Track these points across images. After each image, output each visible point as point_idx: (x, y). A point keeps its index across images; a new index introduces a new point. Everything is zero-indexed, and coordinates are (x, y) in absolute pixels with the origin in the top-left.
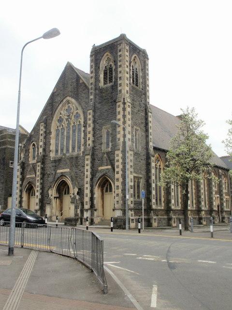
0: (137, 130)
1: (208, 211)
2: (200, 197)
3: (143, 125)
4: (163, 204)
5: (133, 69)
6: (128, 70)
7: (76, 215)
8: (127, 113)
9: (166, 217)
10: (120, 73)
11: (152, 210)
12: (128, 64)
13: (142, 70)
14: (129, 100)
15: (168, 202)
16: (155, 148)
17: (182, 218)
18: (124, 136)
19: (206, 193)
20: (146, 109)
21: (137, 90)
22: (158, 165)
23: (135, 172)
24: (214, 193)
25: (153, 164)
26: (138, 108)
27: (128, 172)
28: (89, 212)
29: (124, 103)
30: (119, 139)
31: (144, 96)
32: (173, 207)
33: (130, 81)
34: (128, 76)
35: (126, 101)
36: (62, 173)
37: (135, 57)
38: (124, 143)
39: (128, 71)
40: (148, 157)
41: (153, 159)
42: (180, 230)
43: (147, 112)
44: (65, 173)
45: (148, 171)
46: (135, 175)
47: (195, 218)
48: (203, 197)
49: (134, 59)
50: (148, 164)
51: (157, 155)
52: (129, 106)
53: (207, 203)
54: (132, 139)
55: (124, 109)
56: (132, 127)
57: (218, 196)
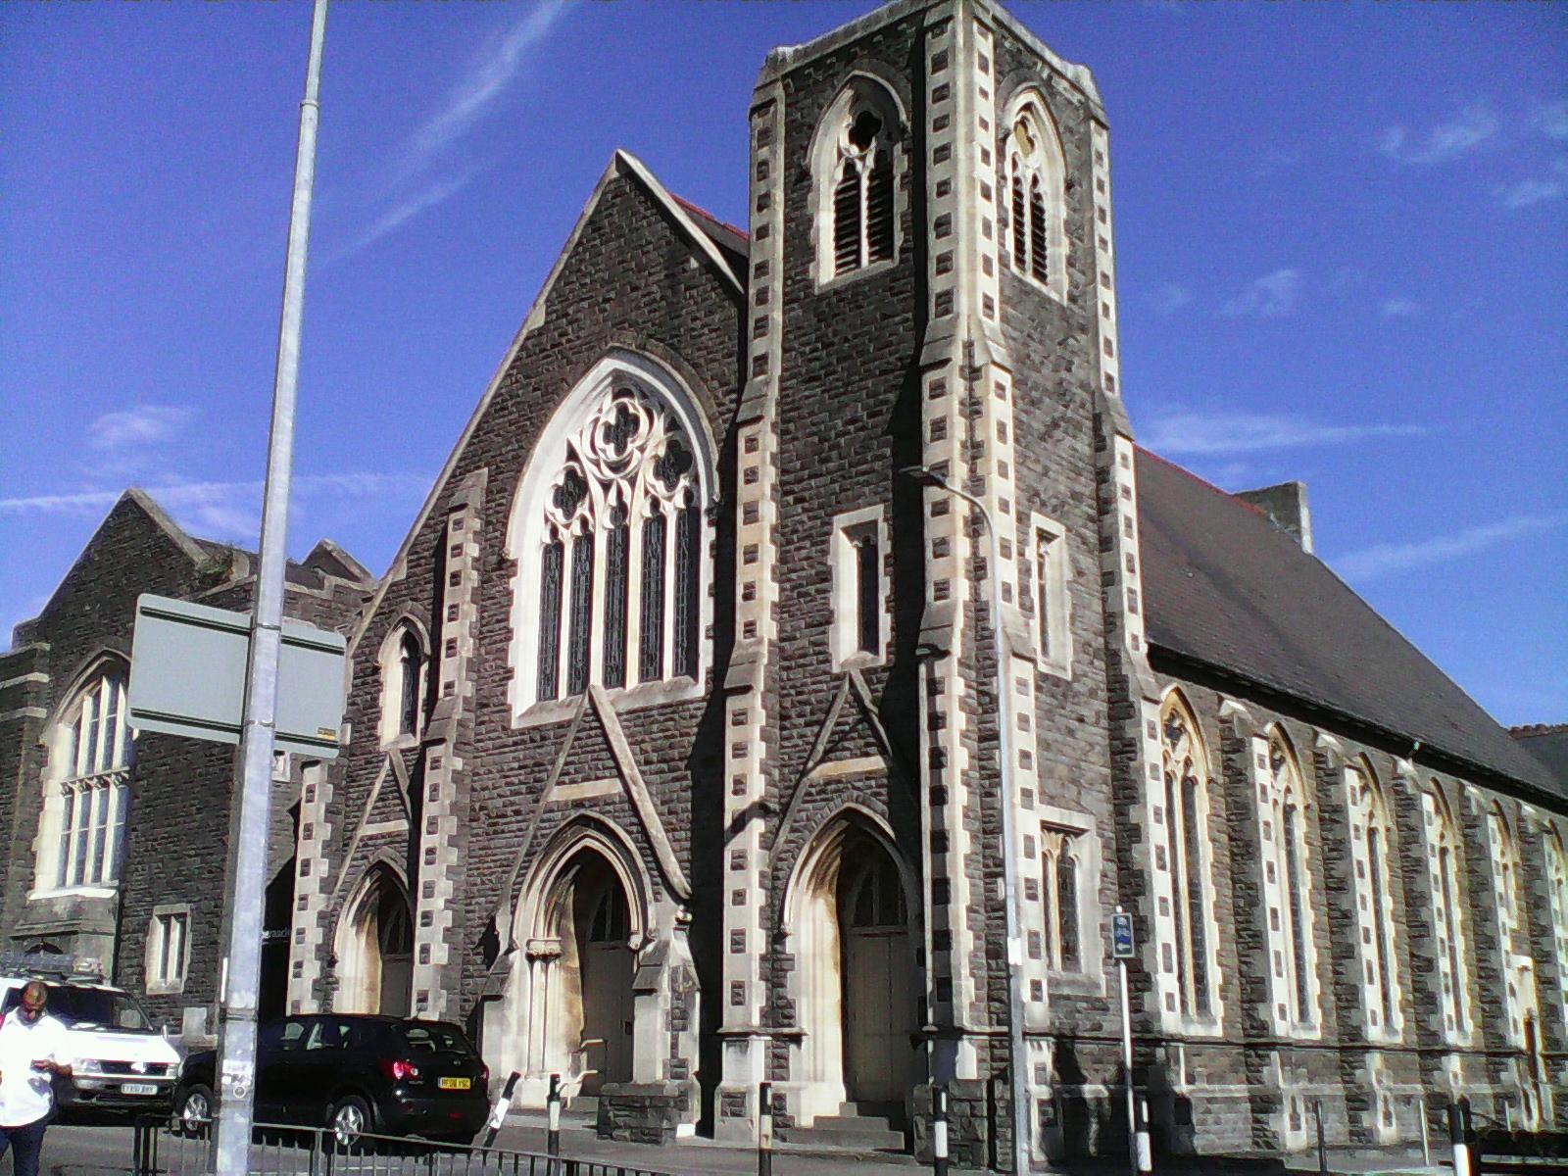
0: (1045, 537)
1: (1477, 1053)
2: (1430, 965)
3: (1088, 508)
4: (1217, 1006)
5: (1017, 181)
6: (987, 174)
7: (677, 1068)
8: (988, 432)
9: (1239, 1090)
10: (940, 194)
11: (1272, 1046)
12: (987, 139)
13: (1069, 186)
14: (1000, 353)
15: (1252, 991)
16: (1162, 659)
17: (1333, 1098)
18: (978, 569)
19: (1390, 928)
20: (1097, 420)
21: (1045, 301)
22: (1180, 754)
23: (1050, 800)
24: (1506, 943)
25: (1152, 750)
26: (1050, 408)
27: (1009, 796)
28: (759, 1048)
29: (973, 373)
30: (942, 590)
31: (1082, 337)
32: (1281, 1029)
33: (1002, 237)
34: (989, 210)
35: (979, 361)
36: (578, 804)
37: (1028, 107)
38: (979, 611)
39: (992, 183)
40: (1120, 708)
41: (1149, 714)
42: (508, 1094)
43: (1106, 430)
44: (594, 802)
45: (1125, 791)
46: (1055, 815)
47: (1407, 1100)
48: (1368, 952)
49: (1023, 122)
50: (1123, 751)
51: (1167, 694)
52: (1000, 387)
53: (1314, 986)
54: (1024, 590)
55: (973, 408)
56: (1022, 519)
57: (1528, 961)
